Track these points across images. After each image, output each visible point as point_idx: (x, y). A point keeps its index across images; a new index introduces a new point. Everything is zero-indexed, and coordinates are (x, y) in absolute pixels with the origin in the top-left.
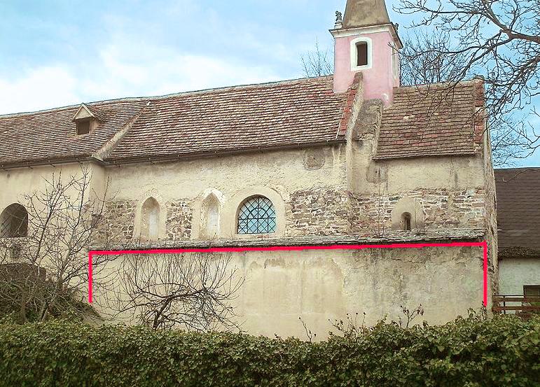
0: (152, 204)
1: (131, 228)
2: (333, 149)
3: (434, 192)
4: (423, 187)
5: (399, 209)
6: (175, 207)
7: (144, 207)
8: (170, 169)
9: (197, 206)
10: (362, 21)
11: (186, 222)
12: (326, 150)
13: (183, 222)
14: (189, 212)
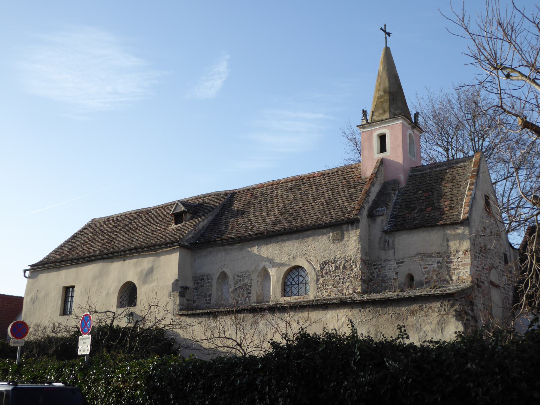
0: (224, 276)
1: (210, 295)
2: (350, 226)
3: (430, 256)
4: (422, 252)
5: (404, 270)
6: (239, 278)
7: (218, 279)
8: (236, 249)
9: (254, 276)
10: (381, 116)
11: (247, 289)
12: (345, 227)
13: (245, 289)
14: (249, 281)
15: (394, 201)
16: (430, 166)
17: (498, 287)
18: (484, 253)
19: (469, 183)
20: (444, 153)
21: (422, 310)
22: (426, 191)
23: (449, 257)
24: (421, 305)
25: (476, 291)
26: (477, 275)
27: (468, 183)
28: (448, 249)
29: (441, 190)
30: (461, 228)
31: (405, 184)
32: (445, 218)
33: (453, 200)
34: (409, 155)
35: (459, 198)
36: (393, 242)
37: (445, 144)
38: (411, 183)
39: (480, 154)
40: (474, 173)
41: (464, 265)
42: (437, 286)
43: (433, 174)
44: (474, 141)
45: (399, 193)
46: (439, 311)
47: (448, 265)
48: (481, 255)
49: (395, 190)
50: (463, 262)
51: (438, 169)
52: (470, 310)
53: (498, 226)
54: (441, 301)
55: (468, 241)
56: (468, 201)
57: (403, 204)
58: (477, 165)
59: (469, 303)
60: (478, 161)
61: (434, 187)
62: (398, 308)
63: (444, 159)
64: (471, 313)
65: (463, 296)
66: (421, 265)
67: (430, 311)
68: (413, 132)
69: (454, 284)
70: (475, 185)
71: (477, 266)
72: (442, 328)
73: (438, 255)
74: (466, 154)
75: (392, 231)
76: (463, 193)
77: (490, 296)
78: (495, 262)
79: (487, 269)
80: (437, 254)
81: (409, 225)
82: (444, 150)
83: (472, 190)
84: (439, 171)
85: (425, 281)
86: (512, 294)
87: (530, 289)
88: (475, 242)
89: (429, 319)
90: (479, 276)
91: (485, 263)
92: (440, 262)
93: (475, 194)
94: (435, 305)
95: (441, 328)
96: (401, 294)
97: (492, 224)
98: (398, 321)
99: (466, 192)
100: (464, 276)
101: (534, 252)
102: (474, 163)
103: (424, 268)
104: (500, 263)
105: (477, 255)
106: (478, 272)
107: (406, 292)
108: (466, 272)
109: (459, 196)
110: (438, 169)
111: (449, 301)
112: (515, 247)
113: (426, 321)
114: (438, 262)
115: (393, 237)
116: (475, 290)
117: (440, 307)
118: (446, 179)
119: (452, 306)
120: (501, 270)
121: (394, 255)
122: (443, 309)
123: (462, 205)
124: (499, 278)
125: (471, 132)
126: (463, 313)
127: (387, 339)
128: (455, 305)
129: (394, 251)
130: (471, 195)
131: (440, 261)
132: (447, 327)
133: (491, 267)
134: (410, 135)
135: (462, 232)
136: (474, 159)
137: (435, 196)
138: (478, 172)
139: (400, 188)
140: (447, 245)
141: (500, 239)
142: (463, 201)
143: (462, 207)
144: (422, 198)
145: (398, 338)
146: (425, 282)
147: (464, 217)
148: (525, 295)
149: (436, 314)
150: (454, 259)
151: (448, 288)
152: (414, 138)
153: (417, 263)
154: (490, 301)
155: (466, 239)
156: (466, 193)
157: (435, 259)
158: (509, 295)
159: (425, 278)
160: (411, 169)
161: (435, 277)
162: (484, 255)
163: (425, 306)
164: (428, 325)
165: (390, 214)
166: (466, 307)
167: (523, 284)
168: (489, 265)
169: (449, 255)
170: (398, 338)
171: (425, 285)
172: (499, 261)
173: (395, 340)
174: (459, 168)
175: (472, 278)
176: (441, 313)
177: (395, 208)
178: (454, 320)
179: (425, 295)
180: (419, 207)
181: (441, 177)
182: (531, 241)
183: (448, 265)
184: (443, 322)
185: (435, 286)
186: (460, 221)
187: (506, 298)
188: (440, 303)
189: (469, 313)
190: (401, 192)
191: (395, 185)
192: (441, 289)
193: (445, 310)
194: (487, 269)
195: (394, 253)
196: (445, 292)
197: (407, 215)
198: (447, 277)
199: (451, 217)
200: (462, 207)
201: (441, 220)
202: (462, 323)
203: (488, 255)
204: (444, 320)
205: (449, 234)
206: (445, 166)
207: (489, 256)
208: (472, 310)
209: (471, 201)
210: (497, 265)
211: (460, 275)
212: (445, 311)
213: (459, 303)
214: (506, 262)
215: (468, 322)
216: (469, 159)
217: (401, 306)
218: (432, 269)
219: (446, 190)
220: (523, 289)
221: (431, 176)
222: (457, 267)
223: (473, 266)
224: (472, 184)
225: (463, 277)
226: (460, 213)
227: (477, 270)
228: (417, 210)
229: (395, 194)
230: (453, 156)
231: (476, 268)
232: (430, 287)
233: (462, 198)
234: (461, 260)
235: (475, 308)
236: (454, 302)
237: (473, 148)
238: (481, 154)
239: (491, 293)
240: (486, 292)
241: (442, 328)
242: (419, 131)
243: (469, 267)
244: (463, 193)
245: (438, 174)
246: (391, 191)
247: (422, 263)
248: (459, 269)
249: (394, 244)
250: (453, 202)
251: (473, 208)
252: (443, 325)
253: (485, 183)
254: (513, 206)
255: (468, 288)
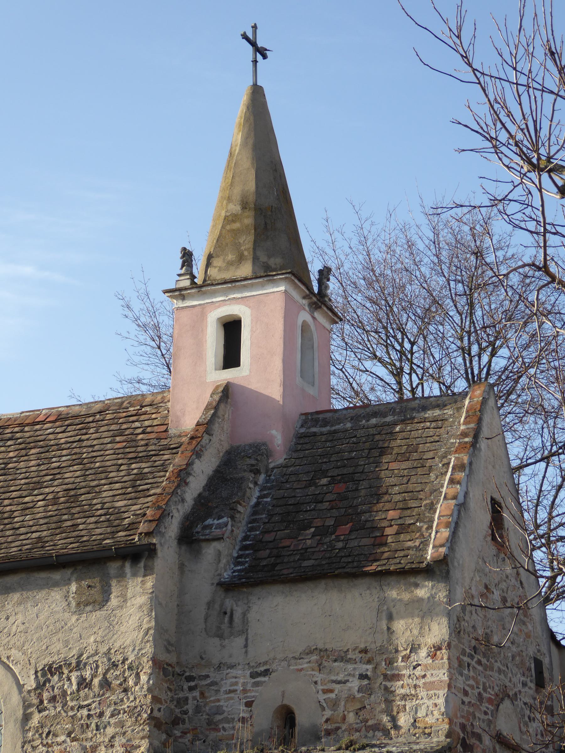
2: (128, 565)
3: (342, 658)
4: (320, 646)
12: (113, 567)
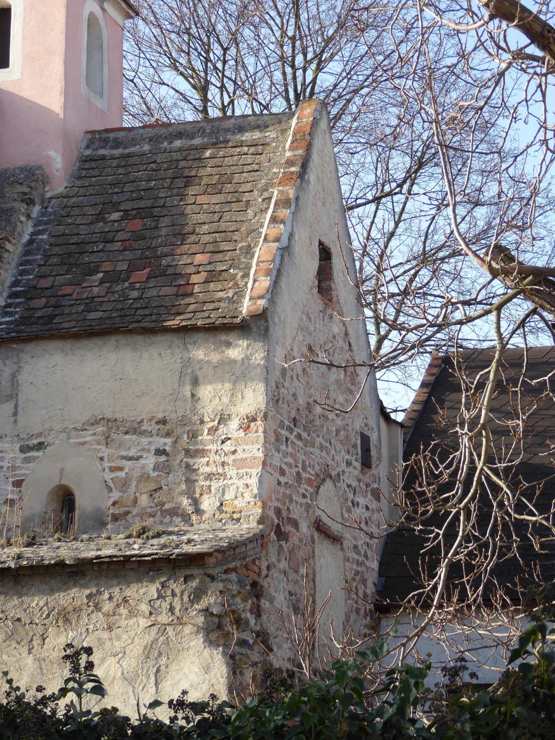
4: (108, 415)
15: (26, 238)
16: (151, 132)
17: (338, 541)
18: (305, 429)
19: (273, 201)
20: (194, 96)
21: (97, 607)
22: (134, 212)
23: (193, 435)
24: (94, 590)
25: (272, 549)
26: (278, 500)
27: (270, 198)
28: (193, 409)
29: (183, 214)
30: (241, 342)
31: (65, 184)
32: (192, 308)
33: (220, 252)
34: (83, 87)
35: (240, 245)
36: (13, 376)
37: (198, 65)
38: (86, 182)
39: (313, 107)
40: (293, 169)
41: (240, 464)
42: (149, 530)
43: (160, 158)
44: (293, 66)
45: (43, 215)
46: (151, 613)
47: (191, 461)
48: (295, 433)
49: (30, 202)
50: (240, 455)
51: (178, 143)
52: (251, 612)
53: (350, 345)
54: (163, 580)
55: (261, 387)
56: (270, 258)
57: (56, 250)
58: (304, 144)
59: (248, 588)
60: (308, 128)
61: (161, 202)
62: (16, 601)
63: (190, 116)
64: (252, 622)
65: (232, 565)
66: (102, 459)
67: (123, 611)
68: (103, 10)
69: (203, 526)
70: (293, 206)
71: (281, 468)
72: (158, 671)
73: (161, 426)
74: (266, 107)
75: (12, 340)
76: (253, 231)
77: (314, 571)
78: (333, 459)
79: (309, 482)
80: (157, 423)
81: (73, 324)
82: (194, 87)
83: (282, 222)
84: (180, 150)
85: (111, 511)
86: (375, 565)
87: (460, 545)
88: (282, 390)
89: (119, 638)
90: (284, 504)
91: (304, 462)
92: (165, 450)
93: (291, 236)
94: (142, 591)
95: (155, 670)
96: (28, 552)
97: (334, 337)
98: (14, 645)
99: (262, 226)
100: (240, 499)
101: (484, 427)
102: (294, 134)
103: (113, 469)
104: (349, 464)
105: (284, 432)
106: (282, 490)
107: (45, 548)
108: (247, 486)
109: (241, 241)
110: (178, 143)
111: (187, 579)
112: (393, 416)
113: (108, 644)
114: (159, 452)
115: (16, 360)
116: (270, 548)
117: (158, 598)
118: (201, 178)
119: (197, 595)
120: (349, 486)
121: (15, 421)
122: (165, 605)
123: (249, 268)
124: (342, 513)
125: (284, 33)
126: (227, 621)
127: (23, 695)
128: (206, 593)
129: (16, 406)
130: (277, 240)
131: (167, 448)
132: (174, 667)
133: (322, 477)
134: (92, 20)
135: (242, 356)
136: (294, 122)
137: (164, 231)
138: (304, 166)
139: (48, 195)
140: (193, 395)
141: (353, 387)
142: (252, 257)
143: (246, 275)
144: (121, 236)
145: (63, 692)
146: (113, 515)
147: (253, 308)
148: (444, 564)
149: (143, 622)
150: (213, 442)
151: (185, 538)
152: (105, 33)
153: (89, 450)
154: (311, 584)
155: (252, 380)
156: (264, 230)
157: (151, 439)
158: (367, 568)
159: (111, 502)
160: (90, 136)
161: (144, 500)
162: (304, 435)
163: (106, 596)
164: (113, 660)
165: (8, 283)
166: (238, 600)
167: (441, 530)
168: (317, 467)
169: (195, 428)
170: (63, 692)
171: (109, 526)
172: (347, 457)
173: (54, 698)
174: (246, 149)
175: (264, 506)
176: (159, 619)
177: (26, 263)
178: (198, 641)
179: (110, 557)
180: (107, 266)
181: (187, 170)
182: (473, 391)
183: (191, 461)
184: (164, 648)
185: (144, 530)
186: (238, 320)
187: (358, 578)
188: (158, 585)
189: (247, 622)
190: (50, 210)
191: (33, 185)
192: (163, 540)
193: (171, 609)
194: (309, 482)
195: (15, 414)
196: (176, 551)
197: (67, 290)
198: (185, 502)
199: (211, 306)
200: (248, 275)
201: (179, 314)
202: (224, 653)
203: (314, 436)
204: (167, 641)
205: (199, 362)
206: (203, 136)
207: (319, 440)
208: (257, 612)
209: (278, 259)
210: (340, 470)
211: (227, 497)
212: (173, 614)
213: (221, 586)
214: (366, 463)
215: (243, 650)
216: (280, 122)
217: (27, 594)
218: (136, 474)
219: (201, 217)
220: (439, 543)
221: (154, 166)
222: (220, 471)
223: (268, 468)
224: (285, 203)
225: (236, 502)
226: (240, 294)
227: (279, 483)
228: (101, 275)
229: (29, 217)
230: (223, 109)
231: (277, 475)
232: (127, 533)
233: (249, 246)
234: (233, 449)
235: (265, 604)
236: (202, 582)
237: (287, 91)
238: (319, 107)
239: (316, 558)
240: (301, 554)
241: (158, 671)
242: (120, 9)
243: (256, 471)
244: (254, 231)
245: (178, 161)
246: (17, 205)
247: (105, 452)
248: (224, 475)
249: (18, 384)
250: (219, 257)
251: (283, 283)
252: (163, 661)
253: (323, 204)
254: (393, 289)
255: (250, 540)
